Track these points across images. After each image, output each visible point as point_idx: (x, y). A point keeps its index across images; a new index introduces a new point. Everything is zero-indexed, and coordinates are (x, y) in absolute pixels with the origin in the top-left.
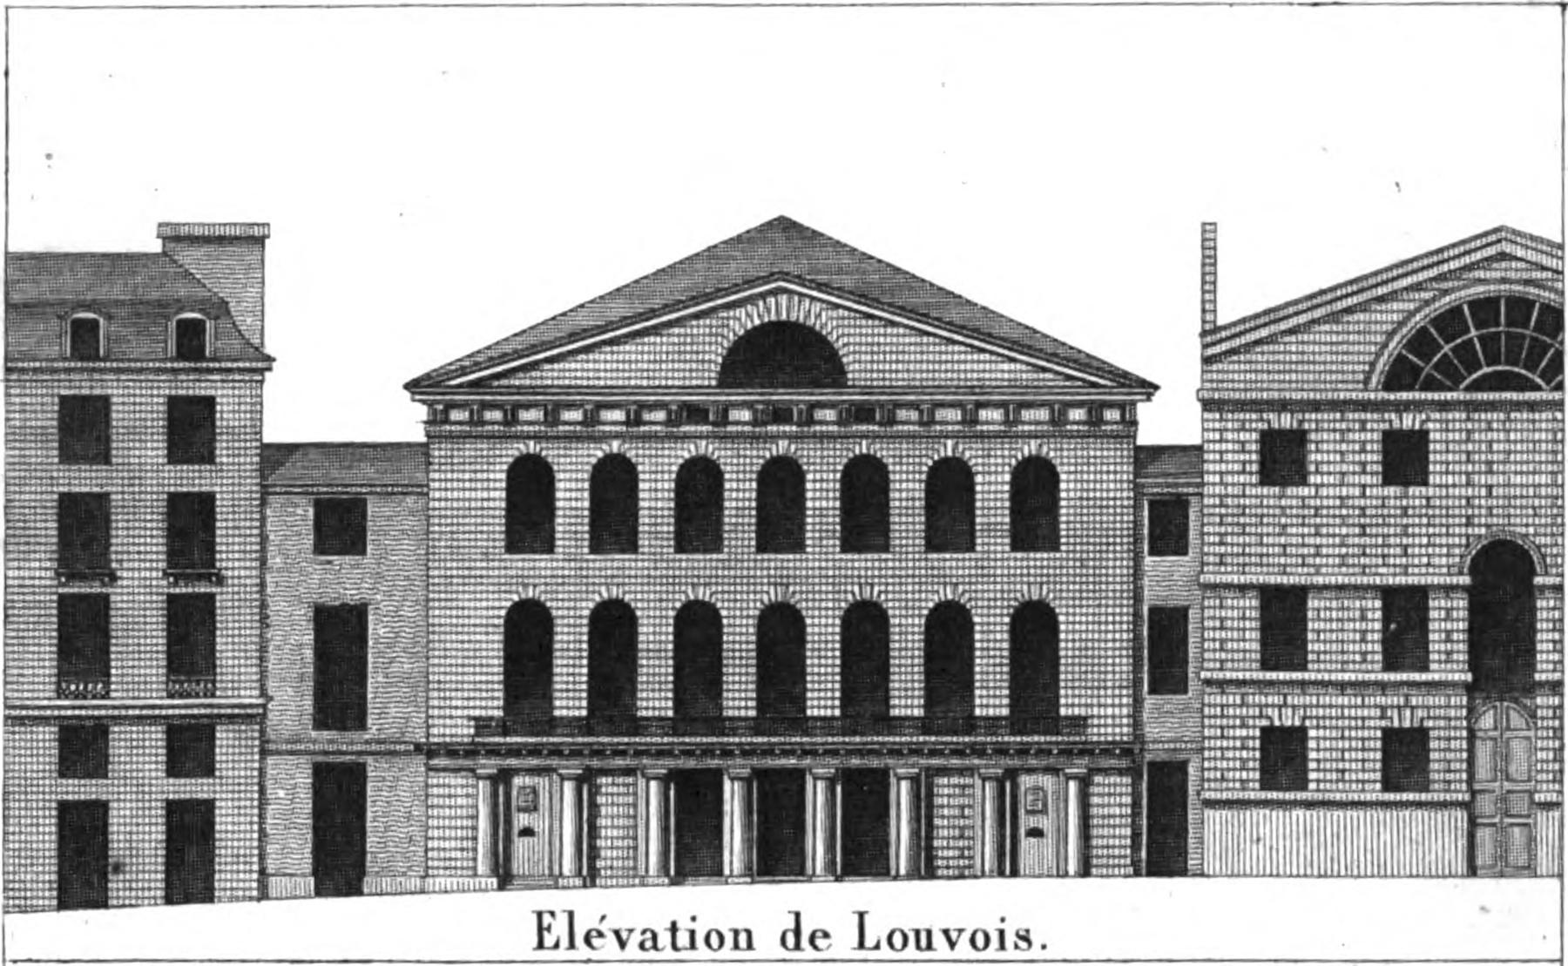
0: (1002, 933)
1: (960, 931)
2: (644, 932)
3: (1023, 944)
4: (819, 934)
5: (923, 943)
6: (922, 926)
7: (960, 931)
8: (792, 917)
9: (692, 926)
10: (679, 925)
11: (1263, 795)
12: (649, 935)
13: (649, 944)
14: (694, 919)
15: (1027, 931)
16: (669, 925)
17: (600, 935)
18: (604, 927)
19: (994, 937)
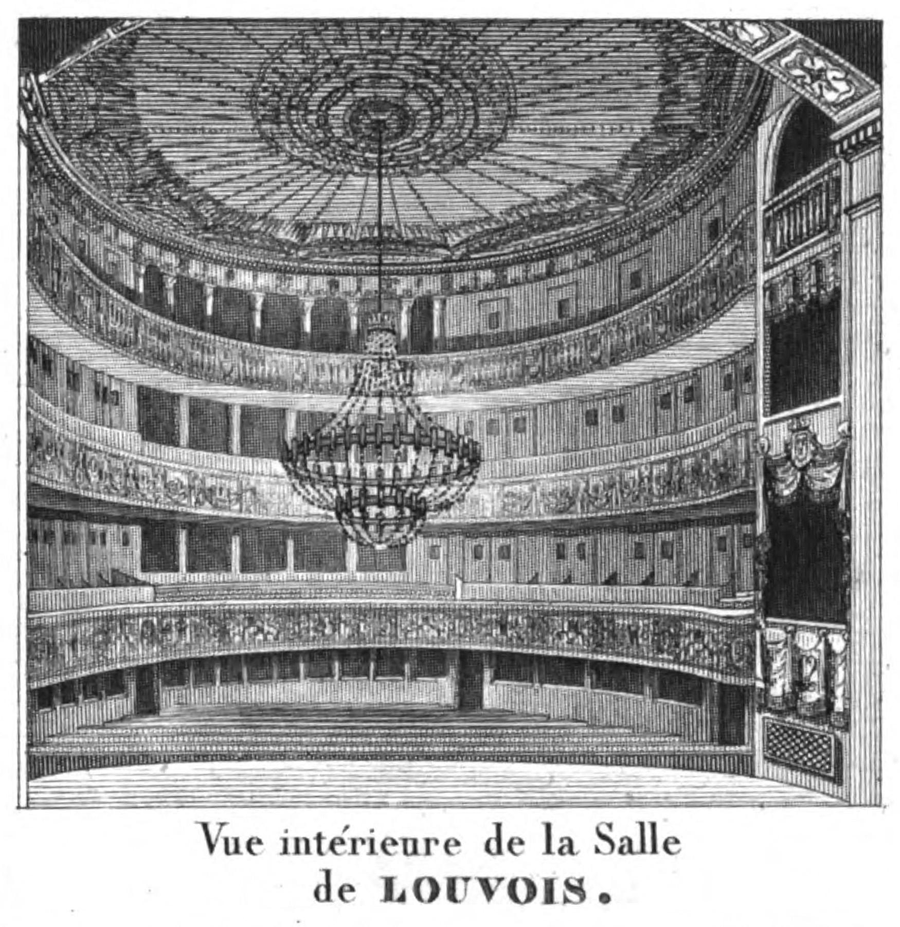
1: (500, 880)
7: (500, 880)
15: (581, 881)
17: (343, 842)
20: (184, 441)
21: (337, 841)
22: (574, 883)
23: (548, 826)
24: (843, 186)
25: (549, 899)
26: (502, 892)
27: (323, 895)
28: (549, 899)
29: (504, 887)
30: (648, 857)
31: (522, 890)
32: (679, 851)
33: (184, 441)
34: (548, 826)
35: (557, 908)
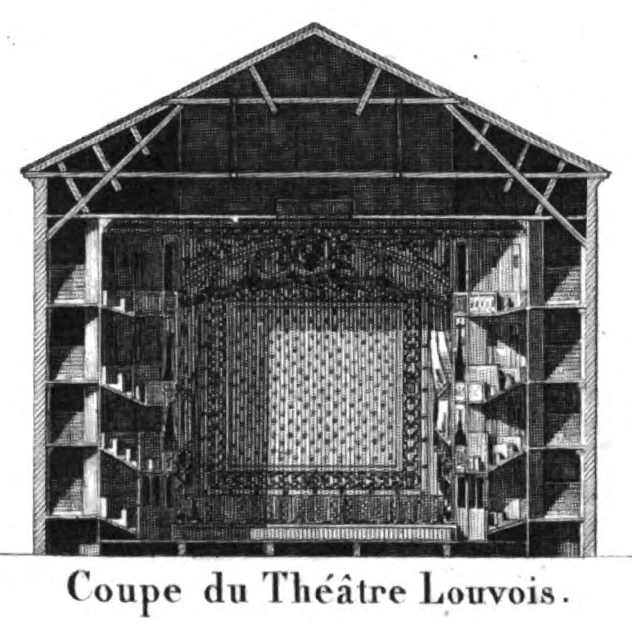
0: (532, 590)
1: (503, 589)
2: (340, 589)
3: (548, 599)
4: (397, 590)
5: (476, 598)
6: (126, 583)
7: (503, 589)
8: (214, 576)
9: (532, 584)
10: (366, 583)
11: (88, 143)
12: (344, 591)
13: (344, 599)
14: (533, 579)
15: (550, 589)
16: (358, 584)
17: (329, 590)
18: (330, 584)
19: (466, 593)
20: (527, 147)
21: (324, 589)
22: (547, 591)
23: (427, 576)
24: (432, 485)
25: (533, 601)
26: (505, 596)
27: (213, 594)
28: (533, 601)
29: (506, 594)
30: (477, 585)
31: (104, 594)
32: (178, 600)
33: (527, 147)
34: (427, 576)
35: (539, 606)
